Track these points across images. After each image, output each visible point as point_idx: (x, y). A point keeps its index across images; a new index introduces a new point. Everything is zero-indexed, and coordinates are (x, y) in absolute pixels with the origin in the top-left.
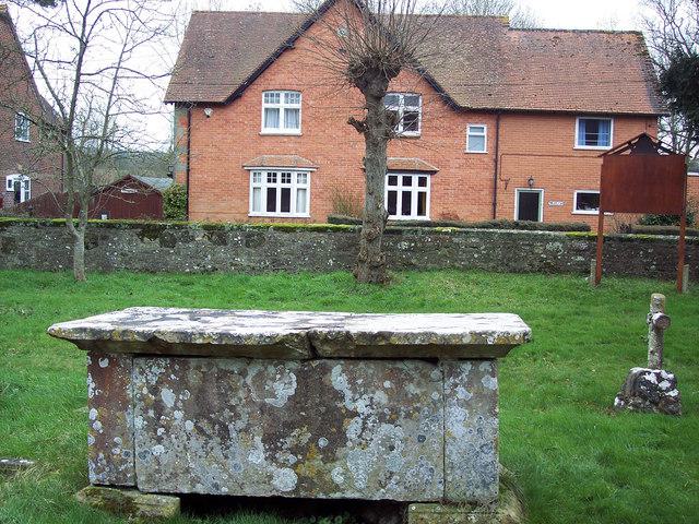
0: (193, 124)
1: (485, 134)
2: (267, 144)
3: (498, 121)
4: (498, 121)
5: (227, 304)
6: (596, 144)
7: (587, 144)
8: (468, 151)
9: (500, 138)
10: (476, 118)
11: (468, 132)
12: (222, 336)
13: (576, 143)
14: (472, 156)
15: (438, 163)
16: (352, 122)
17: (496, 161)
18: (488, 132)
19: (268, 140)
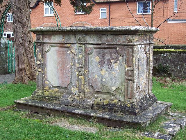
0: (111, 10)
1: (106, 11)
2: (45, 20)
3: (110, 6)
4: (110, 6)
5: (151, 6)
6: (147, 12)
7: (144, 12)
8: (101, 18)
9: (111, 12)
10: (103, 6)
11: (101, 11)
12: (129, 29)
13: (137, 12)
14: (102, 20)
15: (91, 23)
16: (60, 5)
17: (109, 21)
18: (107, 11)
19: (46, 18)
